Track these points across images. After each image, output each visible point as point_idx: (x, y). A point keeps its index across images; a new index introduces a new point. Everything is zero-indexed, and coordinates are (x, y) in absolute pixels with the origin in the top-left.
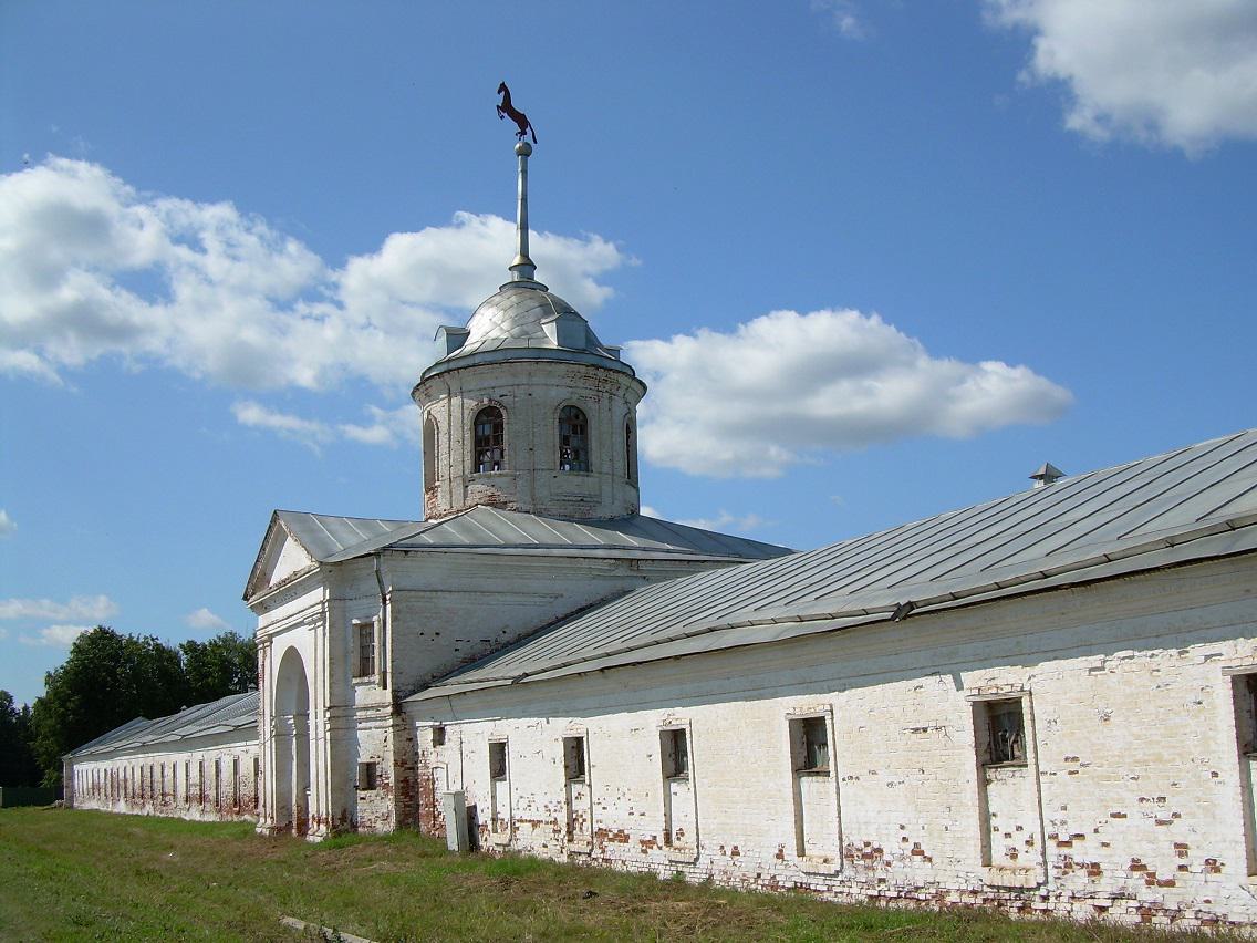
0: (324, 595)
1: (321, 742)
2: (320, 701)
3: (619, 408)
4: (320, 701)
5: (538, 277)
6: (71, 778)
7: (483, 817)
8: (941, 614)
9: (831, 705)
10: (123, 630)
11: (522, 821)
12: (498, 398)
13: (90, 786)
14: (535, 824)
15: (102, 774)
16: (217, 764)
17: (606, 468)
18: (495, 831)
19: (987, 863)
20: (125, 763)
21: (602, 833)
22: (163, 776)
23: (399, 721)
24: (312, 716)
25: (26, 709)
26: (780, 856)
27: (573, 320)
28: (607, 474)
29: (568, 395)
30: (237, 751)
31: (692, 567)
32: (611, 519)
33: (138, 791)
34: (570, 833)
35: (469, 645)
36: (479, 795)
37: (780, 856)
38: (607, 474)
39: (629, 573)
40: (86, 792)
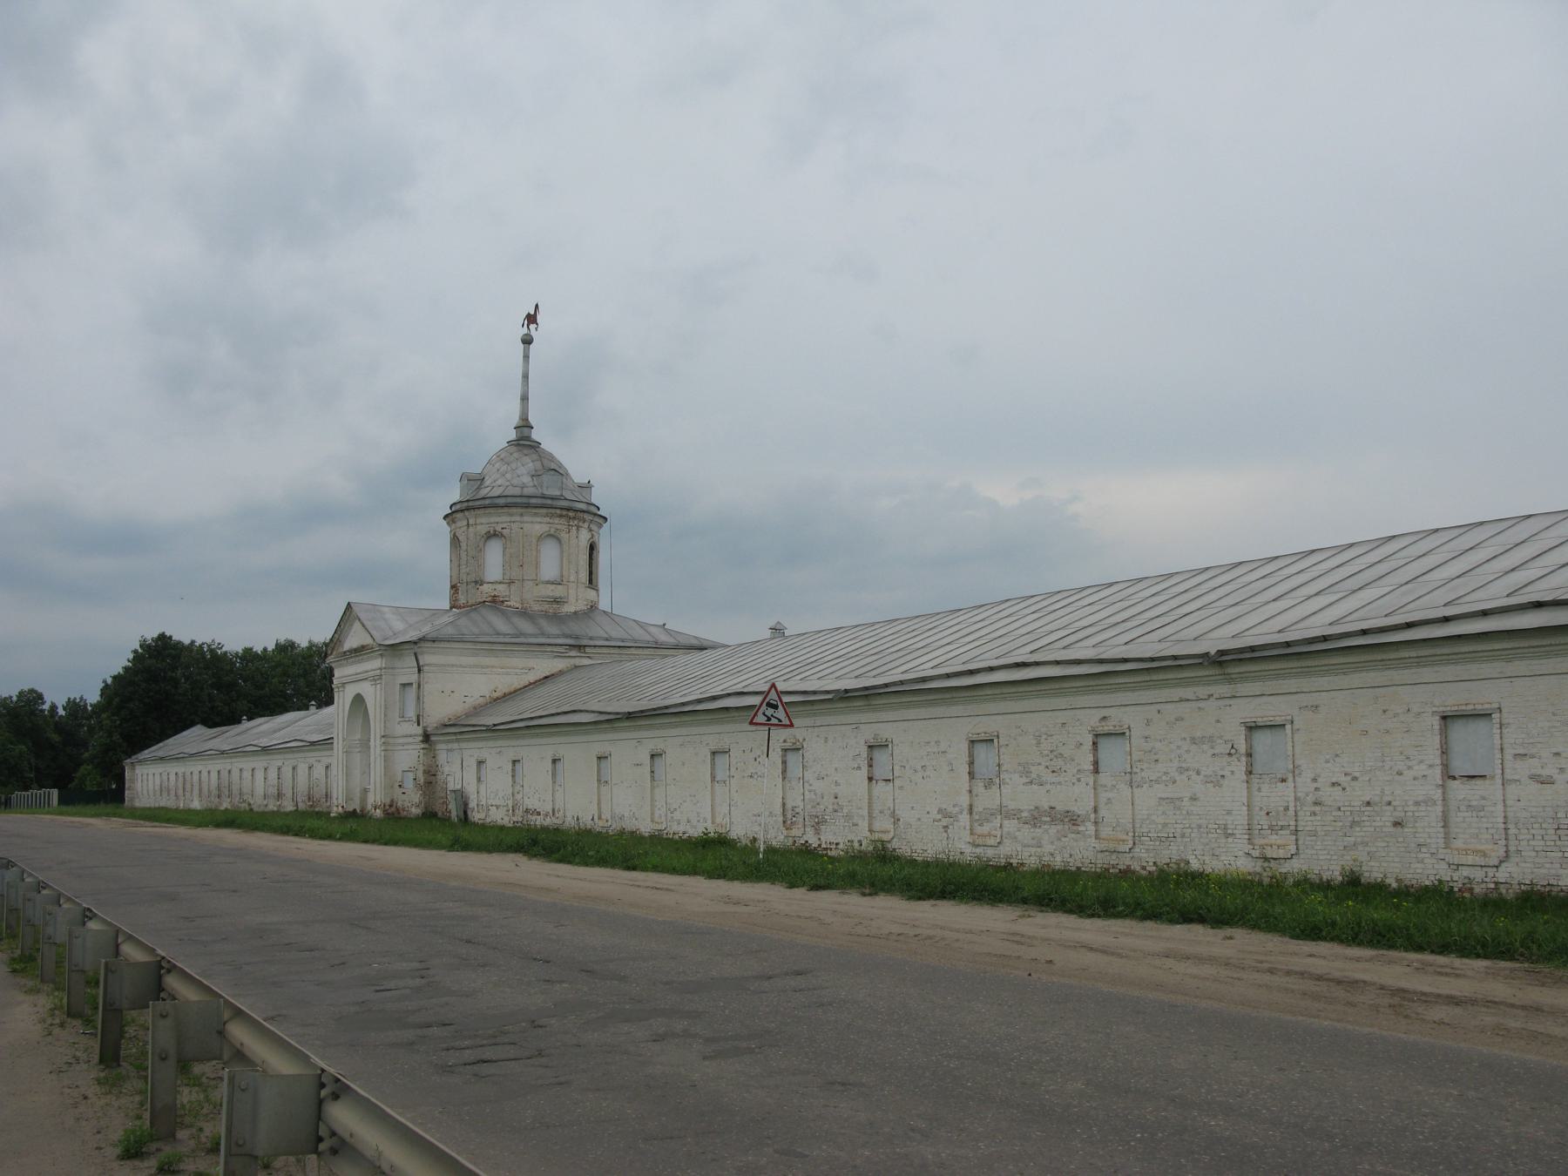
0: (381, 664)
1: (378, 760)
2: (378, 731)
3: (584, 536)
4: (378, 731)
5: (535, 435)
6: (132, 781)
7: (472, 804)
8: (1377, 577)
9: (998, 732)
10: (183, 634)
11: (492, 806)
12: (500, 530)
13: (157, 788)
14: (497, 807)
15: (172, 777)
16: (184, 773)
17: (572, 579)
18: (478, 812)
19: (652, 821)
20: (200, 768)
21: (527, 811)
22: (241, 779)
23: (426, 746)
24: (372, 740)
25: (54, 708)
26: (593, 819)
27: (553, 475)
28: (573, 582)
29: (548, 529)
30: (312, 761)
31: (477, 710)
32: (575, 613)
33: (215, 792)
34: (513, 811)
35: (472, 700)
36: (471, 789)
37: (593, 819)
38: (573, 582)
39: (579, 654)
40: (151, 793)
